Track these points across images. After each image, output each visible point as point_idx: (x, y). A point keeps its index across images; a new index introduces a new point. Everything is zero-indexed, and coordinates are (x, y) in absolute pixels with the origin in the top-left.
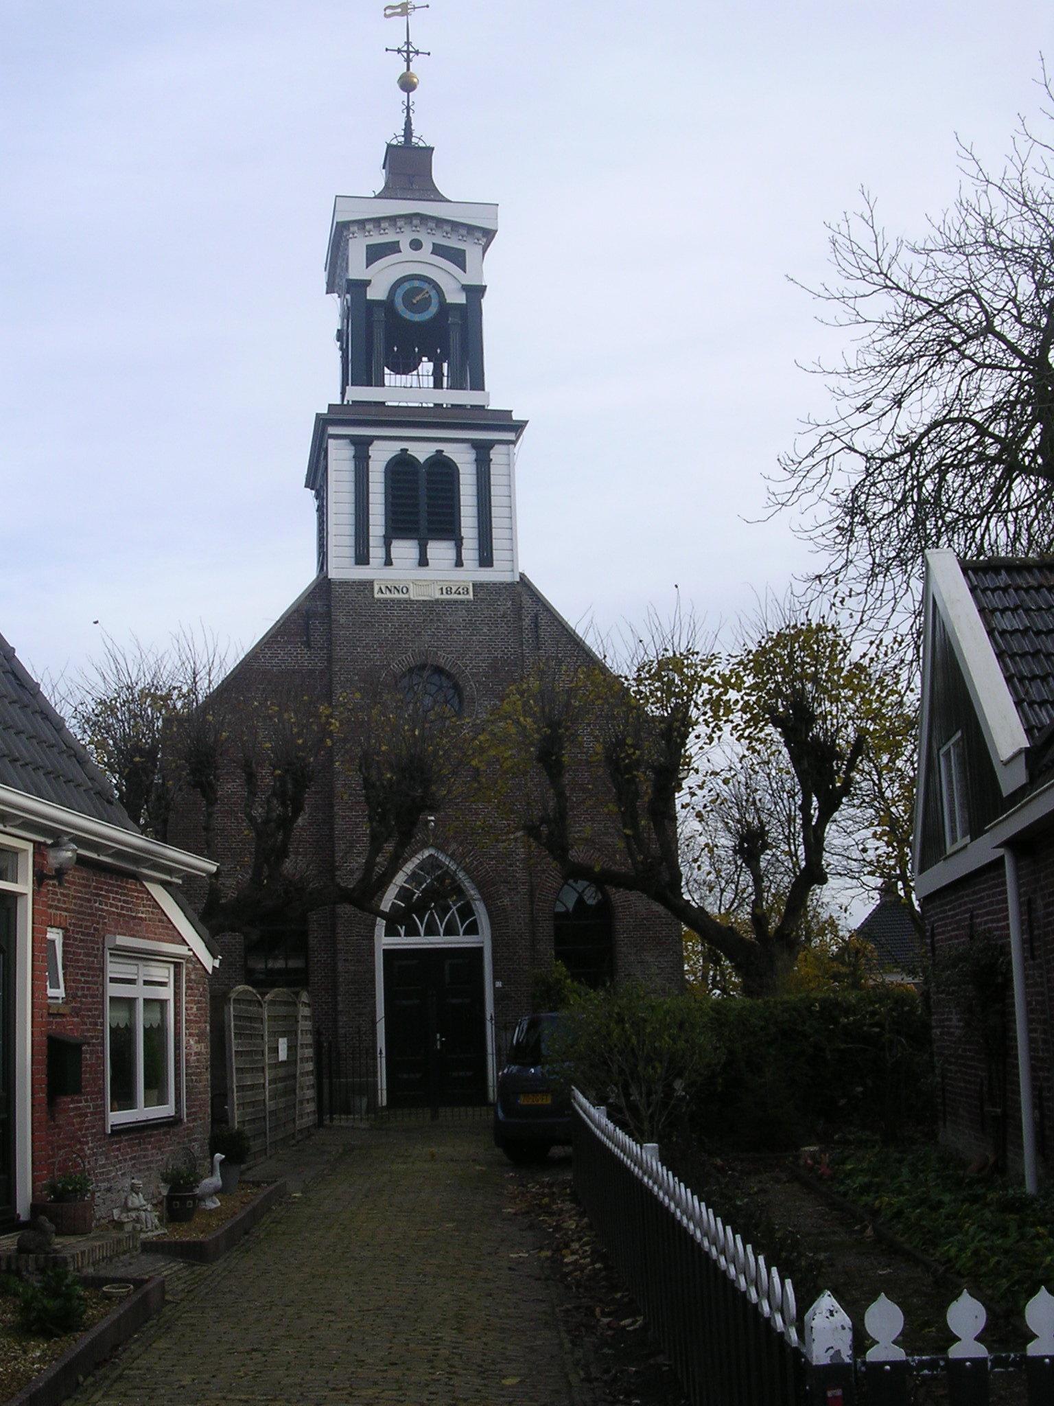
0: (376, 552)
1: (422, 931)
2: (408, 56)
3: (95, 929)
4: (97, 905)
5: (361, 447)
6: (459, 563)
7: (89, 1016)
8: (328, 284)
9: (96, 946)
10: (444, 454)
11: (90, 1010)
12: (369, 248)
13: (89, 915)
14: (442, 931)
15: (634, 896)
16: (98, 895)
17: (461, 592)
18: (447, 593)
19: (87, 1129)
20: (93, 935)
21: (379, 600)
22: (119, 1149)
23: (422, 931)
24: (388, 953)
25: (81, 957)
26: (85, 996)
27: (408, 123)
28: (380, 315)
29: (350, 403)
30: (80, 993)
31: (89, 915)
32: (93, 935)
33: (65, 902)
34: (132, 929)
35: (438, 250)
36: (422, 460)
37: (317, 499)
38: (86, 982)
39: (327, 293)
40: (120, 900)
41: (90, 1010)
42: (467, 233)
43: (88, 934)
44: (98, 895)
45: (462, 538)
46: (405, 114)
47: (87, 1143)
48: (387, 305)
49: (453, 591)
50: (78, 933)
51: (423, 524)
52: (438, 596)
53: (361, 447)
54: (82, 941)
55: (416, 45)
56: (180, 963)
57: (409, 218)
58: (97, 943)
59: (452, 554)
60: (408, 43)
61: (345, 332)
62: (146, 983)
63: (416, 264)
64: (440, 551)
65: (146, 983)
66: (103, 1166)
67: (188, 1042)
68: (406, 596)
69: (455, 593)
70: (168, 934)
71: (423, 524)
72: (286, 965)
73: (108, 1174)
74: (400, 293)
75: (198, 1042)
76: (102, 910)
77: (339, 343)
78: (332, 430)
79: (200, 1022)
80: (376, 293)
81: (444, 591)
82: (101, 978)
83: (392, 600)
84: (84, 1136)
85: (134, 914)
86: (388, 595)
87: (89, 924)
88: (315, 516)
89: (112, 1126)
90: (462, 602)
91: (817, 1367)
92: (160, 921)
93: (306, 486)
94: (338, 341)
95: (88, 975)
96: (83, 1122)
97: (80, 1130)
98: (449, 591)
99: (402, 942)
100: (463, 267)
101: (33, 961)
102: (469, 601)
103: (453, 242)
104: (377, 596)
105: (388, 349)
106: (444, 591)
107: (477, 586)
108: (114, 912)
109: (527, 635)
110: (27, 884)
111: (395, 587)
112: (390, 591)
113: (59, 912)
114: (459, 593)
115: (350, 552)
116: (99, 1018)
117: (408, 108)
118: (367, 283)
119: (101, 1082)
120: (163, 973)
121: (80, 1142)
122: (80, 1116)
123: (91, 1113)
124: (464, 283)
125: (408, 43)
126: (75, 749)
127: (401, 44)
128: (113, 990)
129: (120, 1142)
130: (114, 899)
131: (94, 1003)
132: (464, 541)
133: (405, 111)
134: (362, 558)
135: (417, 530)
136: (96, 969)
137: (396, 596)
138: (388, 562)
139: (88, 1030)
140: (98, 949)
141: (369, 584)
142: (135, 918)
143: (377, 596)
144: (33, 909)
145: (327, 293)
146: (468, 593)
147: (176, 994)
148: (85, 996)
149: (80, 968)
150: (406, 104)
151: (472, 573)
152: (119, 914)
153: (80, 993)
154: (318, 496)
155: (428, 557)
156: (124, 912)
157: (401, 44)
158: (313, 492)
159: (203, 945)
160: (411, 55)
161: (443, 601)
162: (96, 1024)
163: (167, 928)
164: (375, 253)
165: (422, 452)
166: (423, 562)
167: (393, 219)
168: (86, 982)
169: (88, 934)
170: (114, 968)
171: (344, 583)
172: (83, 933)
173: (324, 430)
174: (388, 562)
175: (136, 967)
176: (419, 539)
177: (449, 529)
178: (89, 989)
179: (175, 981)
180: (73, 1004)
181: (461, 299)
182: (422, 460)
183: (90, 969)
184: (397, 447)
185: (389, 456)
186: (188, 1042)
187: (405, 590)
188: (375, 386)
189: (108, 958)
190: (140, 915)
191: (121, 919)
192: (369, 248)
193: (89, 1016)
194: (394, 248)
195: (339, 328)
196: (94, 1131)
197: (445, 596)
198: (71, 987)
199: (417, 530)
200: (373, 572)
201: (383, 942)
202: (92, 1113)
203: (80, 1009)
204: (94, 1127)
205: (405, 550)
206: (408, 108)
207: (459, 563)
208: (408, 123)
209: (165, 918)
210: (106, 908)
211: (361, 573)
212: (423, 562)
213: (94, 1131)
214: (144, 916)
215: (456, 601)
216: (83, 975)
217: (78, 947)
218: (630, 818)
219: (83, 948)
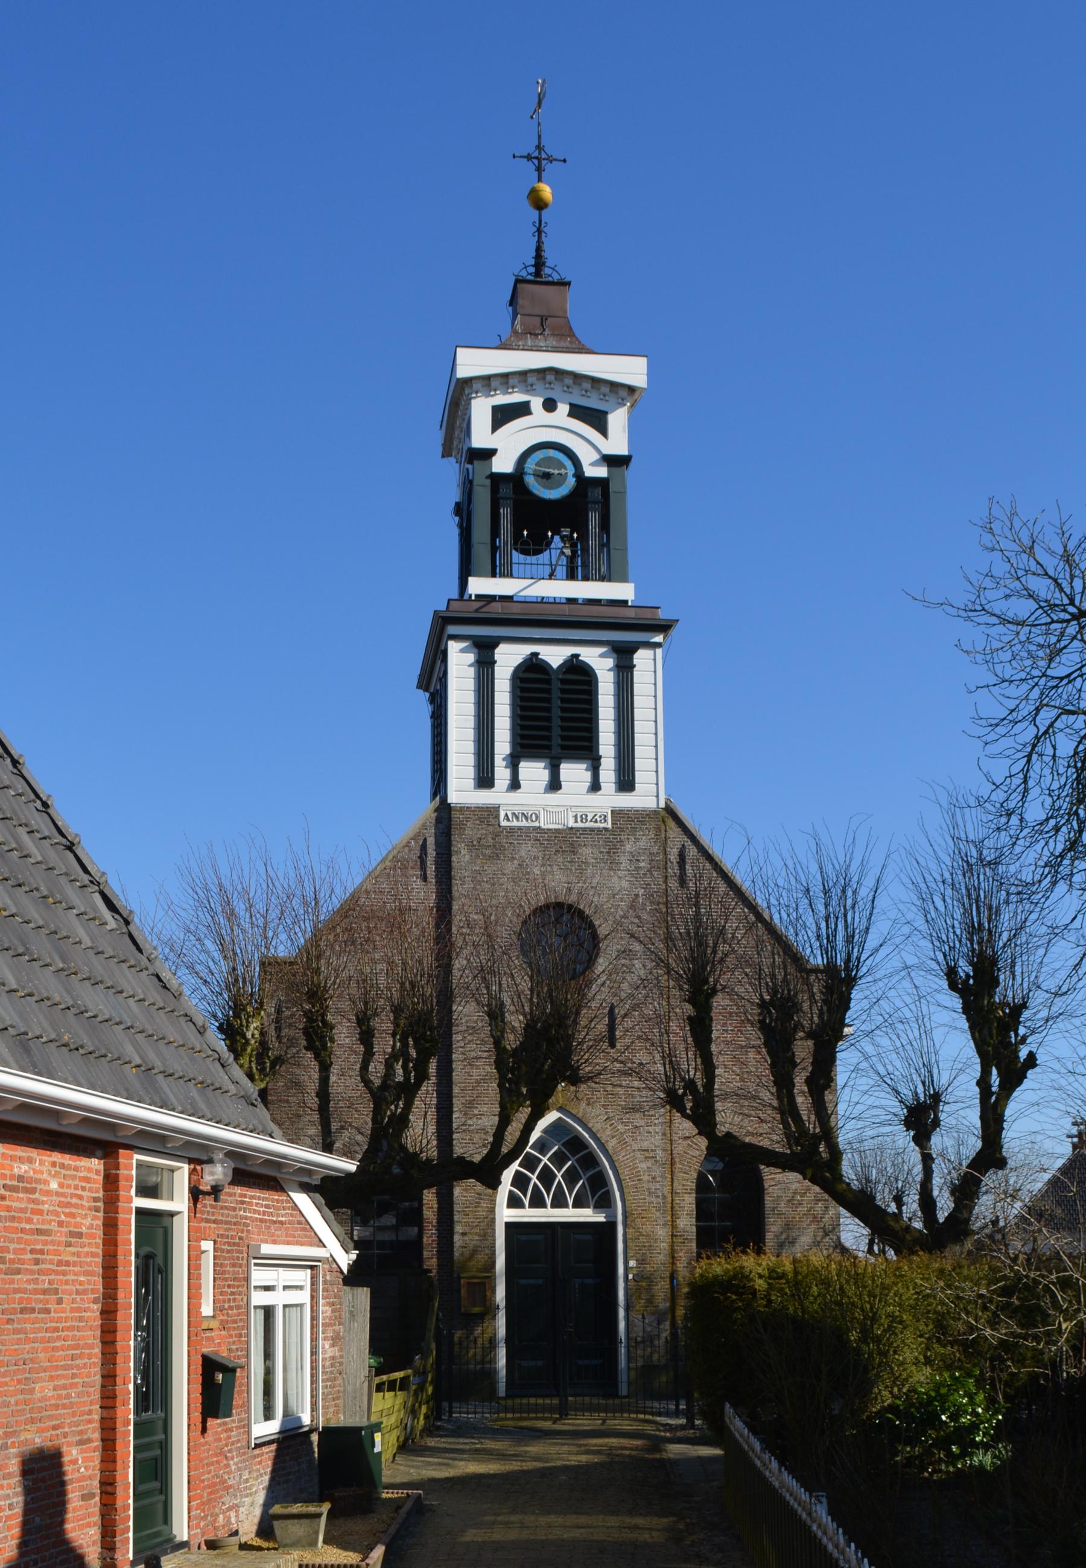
0: (502, 774)
1: (549, 1202)
2: (540, 163)
3: (241, 1238)
4: (241, 1213)
5: (484, 652)
6: (595, 786)
7: (234, 1328)
8: (444, 445)
9: (241, 1256)
10: (580, 658)
11: (235, 1322)
12: (496, 409)
13: (235, 1224)
14: (570, 1203)
15: (793, 1179)
16: (243, 1202)
17: (598, 820)
18: (582, 821)
19: (233, 1443)
20: (238, 1245)
21: (505, 828)
22: (260, 1463)
23: (549, 1202)
24: (510, 1226)
25: (228, 1268)
26: (231, 1308)
27: (539, 249)
28: (506, 491)
29: (473, 598)
30: (226, 1305)
31: (235, 1224)
32: (238, 1245)
33: (213, 1214)
34: (273, 1235)
35: (576, 412)
36: (555, 665)
37: (431, 703)
38: (233, 1293)
39: (443, 456)
40: (262, 1206)
41: (235, 1322)
42: (610, 391)
43: (234, 1244)
44: (243, 1202)
45: (600, 757)
46: (536, 239)
47: (233, 1458)
48: (516, 479)
49: (589, 818)
50: (225, 1243)
51: (556, 741)
52: (571, 823)
53: (484, 652)
54: (228, 1251)
55: (550, 149)
56: (316, 1266)
57: (542, 372)
58: (241, 1252)
59: (588, 776)
60: (539, 147)
61: (465, 507)
62: (285, 1288)
63: (554, 430)
64: (574, 773)
65: (285, 1288)
66: (247, 1481)
67: (323, 1344)
68: (536, 824)
69: (591, 821)
70: (306, 1236)
71: (556, 741)
72: (397, 1236)
73: (250, 1489)
74: (530, 465)
75: (332, 1345)
76: (246, 1218)
77: (457, 519)
78: (452, 629)
79: (335, 1325)
80: (504, 464)
81: (579, 819)
82: (245, 1288)
83: (520, 828)
84: (230, 1451)
85: (275, 1219)
86: (515, 823)
87: (234, 1233)
88: (427, 723)
89: (255, 1439)
90: (599, 830)
91: (480, 1162)
92: (299, 1223)
93: (419, 687)
94: (456, 515)
95: (234, 1286)
96: (229, 1437)
97: (227, 1445)
98: (584, 818)
99: (529, 1215)
100: (603, 430)
101: (189, 1279)
102: (606, 829)
103: (592, 402)
104: (504, 823)
105: (517, 536)
106: (579, 819)
107: (617, 813)
108: (256, 1218)
109: (674, 869)
110: (183, 1202)
111: (523, 814)
112: (517, 818)
113: (208, 1225)
114: (596, 821)
115: (471, 772)
116: (243, 1330)
117: (539, 231)
118: (489, 453)
119: (246, 1395)
120: (303, 1277)
121: (226, 1458)
122: (226, 1431)
123: (236, 1427)
124: (605, 452)
125: (539, 147)
126: (220, 1052)
127: (531, 149)
128: (259, 1299)
129: (262, 1455)
130: (257, 1204)
131: (239, 1314)
132: (602, 760)
133: (536, 234)
134: (485, 779)
135: (549, 747)
136: (239, 1279)
137: (524, 823)
138: (515, 784)
139: (234, 1343)
140: (243, 1258)
141: (492, 812)
142: (275, 1222)
143: (504, 823)
144: (189, 1226)
145: (443, 456)
146: (605, 821)
147: (312, 1297)
148: (231, 1308)
149: (226, 1279)
150: (537, 225)
151: (610, 799)
152: (261, 1220)
153: (226, 1305)
154: (432, 700)
155: (561, 779)
156: (266, 1217)
157: (531, 149)
158: (427, 695)
159: (339, 1244)
160: (544, 162)
161: (578, 829)
162: (240, 1336)
163: (305, 1229)
164: (502, 416)
165: (555, 656)
166: (554, 785)
167: (524, 374)
168: (233, 1293)
169: (234, 1244)
170: (259, 1276)
171: (463, 809)
172: (229, 1244)
173: (442, 630)
174: (515, 784)
175: (94, 1165)
176: (551, 758)
177: (587, 751)
178: (234, 1300)
179: (312, 1284)
180: (222, 1317)
181: (602, 472)
182: (555, 665)
183: (235, 1279)
184: (527, 650)
185: (518, 660)
186: (323, 1344)
187: (534, 818)
188: (500, 576)
189: (253, 1268)
190: (280, 1219)
191: (263, 1225)
192: (496, 409)
193: (234, 1328)
194: (522, 410)
195: (458, 500)
196: (239, 1445)
197: (580, 825)
198: (219, 1301)
199: (549, 747)
200: (497, 796)
201: (506, 1214)
202: (238, 1428)
203: (227, 1322)
204: (239, 1441)
205: (534, 771)
206: (539, 231)
207: (595, 786)
208: (539, 249)
209: (303, 1219)
210: (249, 1215)
211: (484, 798)
212: (554, 785)
213: (239, 1445)
214: (283, 1219)
215: (592, 829)
216: (229, 1286)
217: (225, 1258)
218: (783, 1083)
219: (229, 1258)
